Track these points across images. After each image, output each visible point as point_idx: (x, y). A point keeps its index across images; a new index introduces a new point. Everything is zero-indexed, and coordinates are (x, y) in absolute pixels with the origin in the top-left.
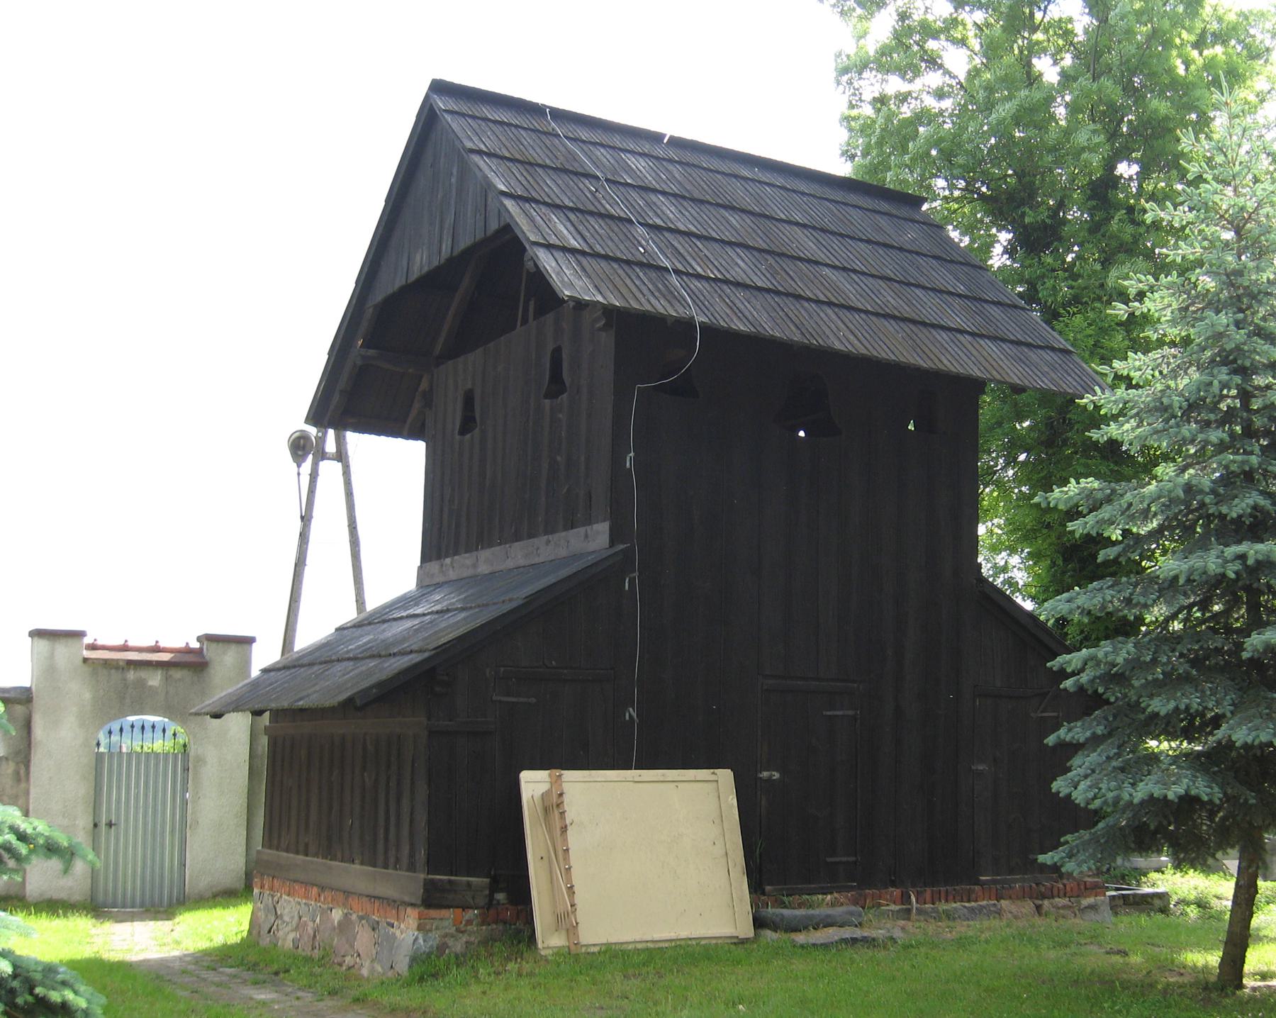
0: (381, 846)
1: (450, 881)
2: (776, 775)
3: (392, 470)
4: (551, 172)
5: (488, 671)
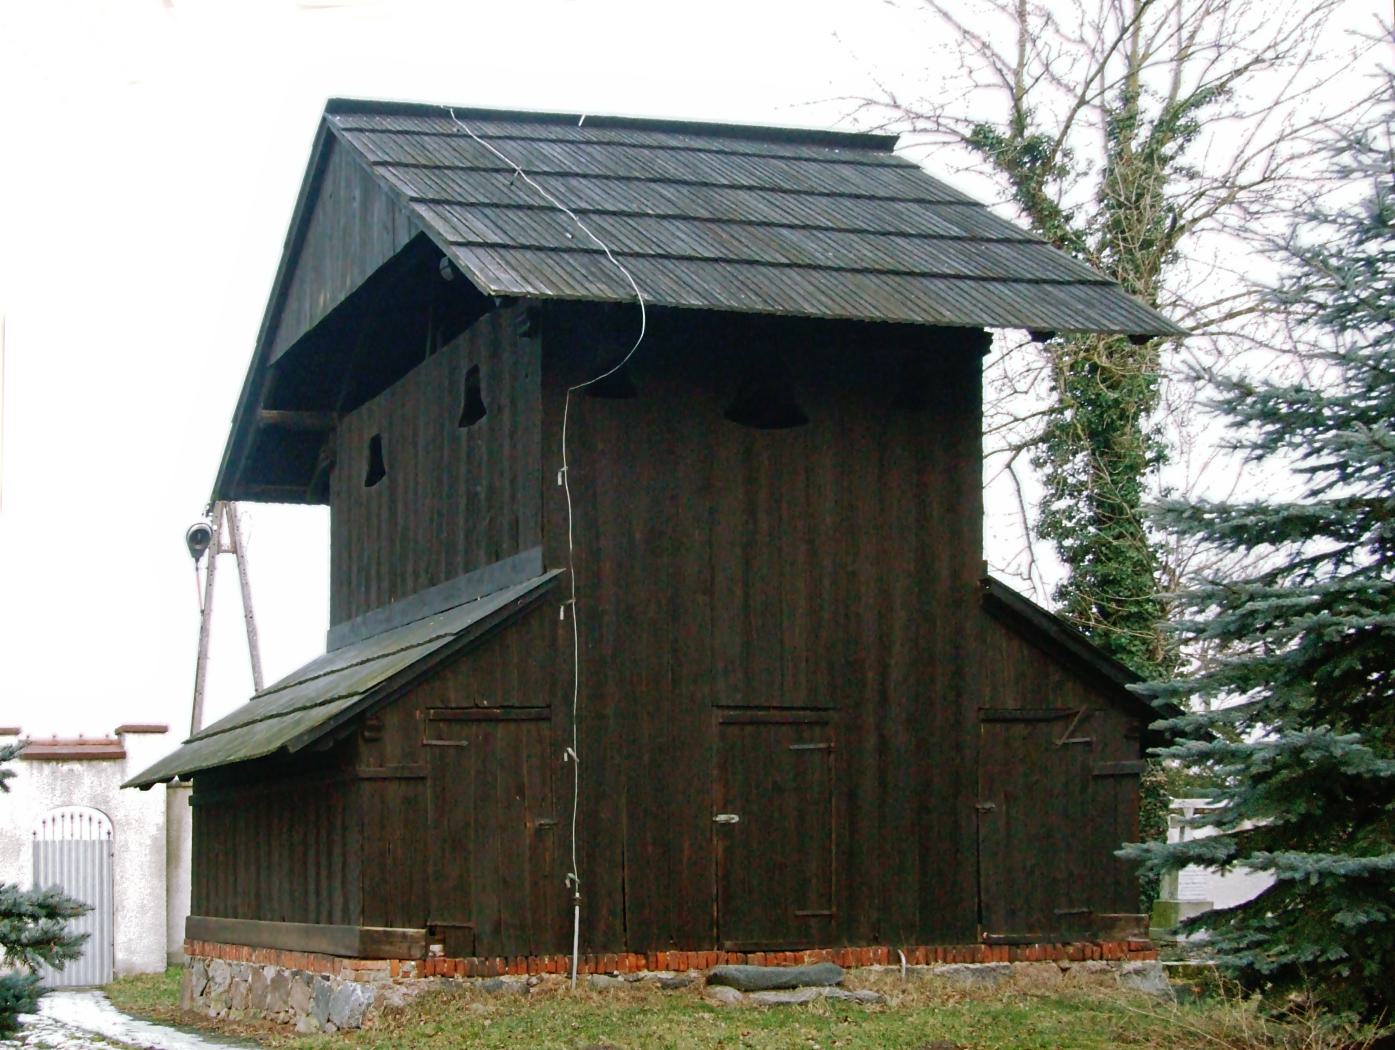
0: (312, 899)
1: (385, 932)
2: (735, 819)
3: (294, 540)
4: (460, 173)
5: (418, 713)
